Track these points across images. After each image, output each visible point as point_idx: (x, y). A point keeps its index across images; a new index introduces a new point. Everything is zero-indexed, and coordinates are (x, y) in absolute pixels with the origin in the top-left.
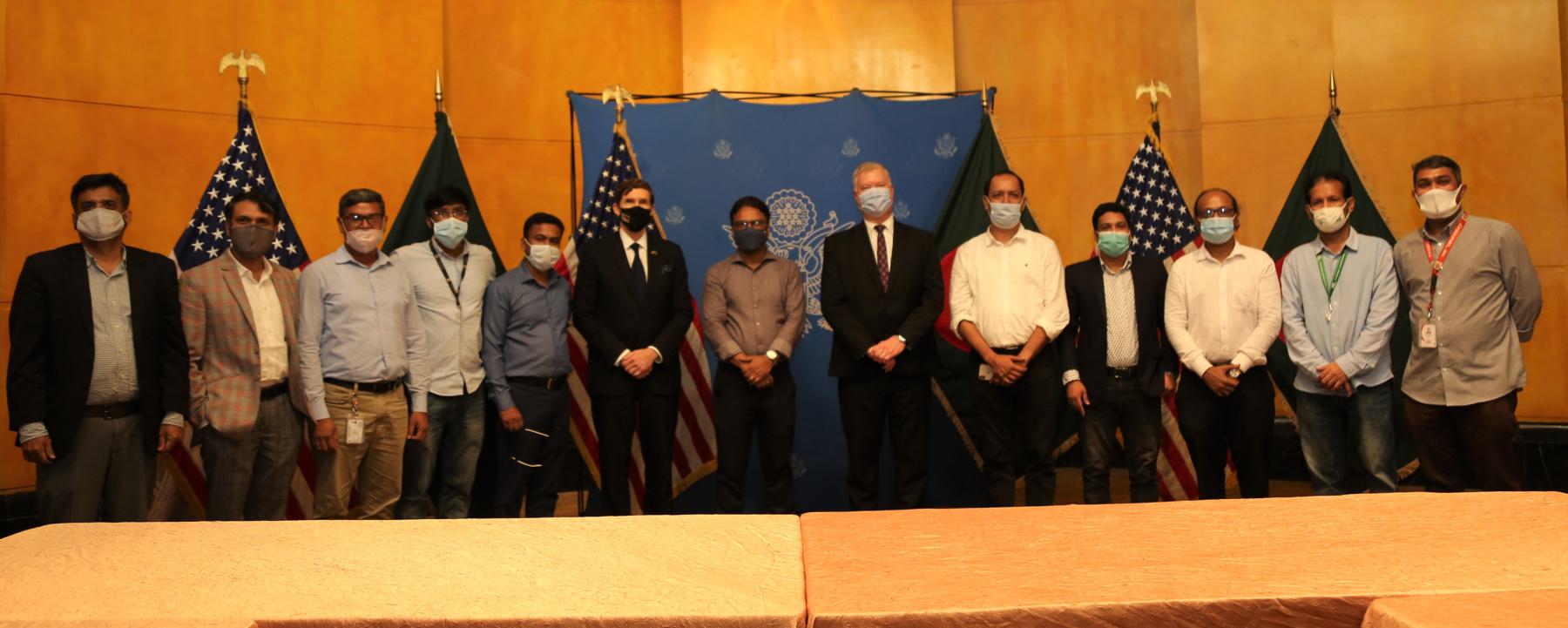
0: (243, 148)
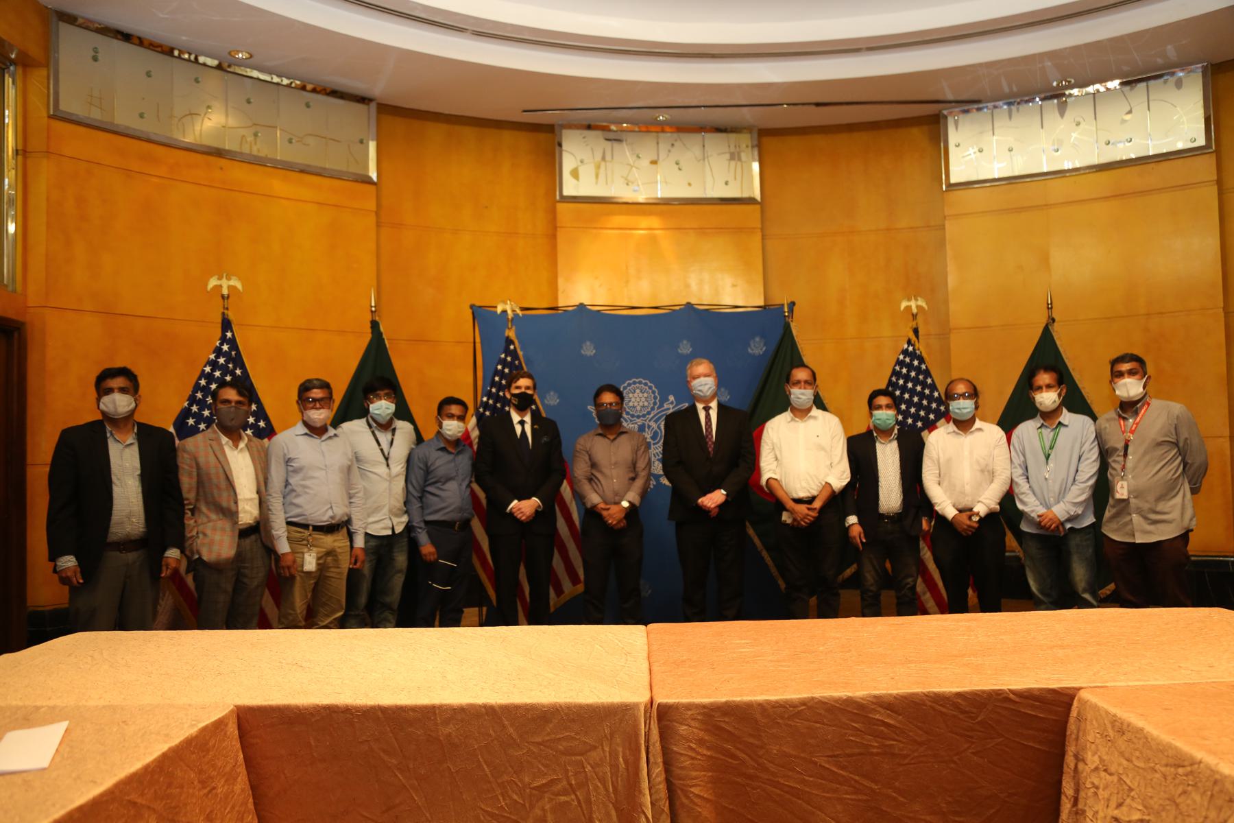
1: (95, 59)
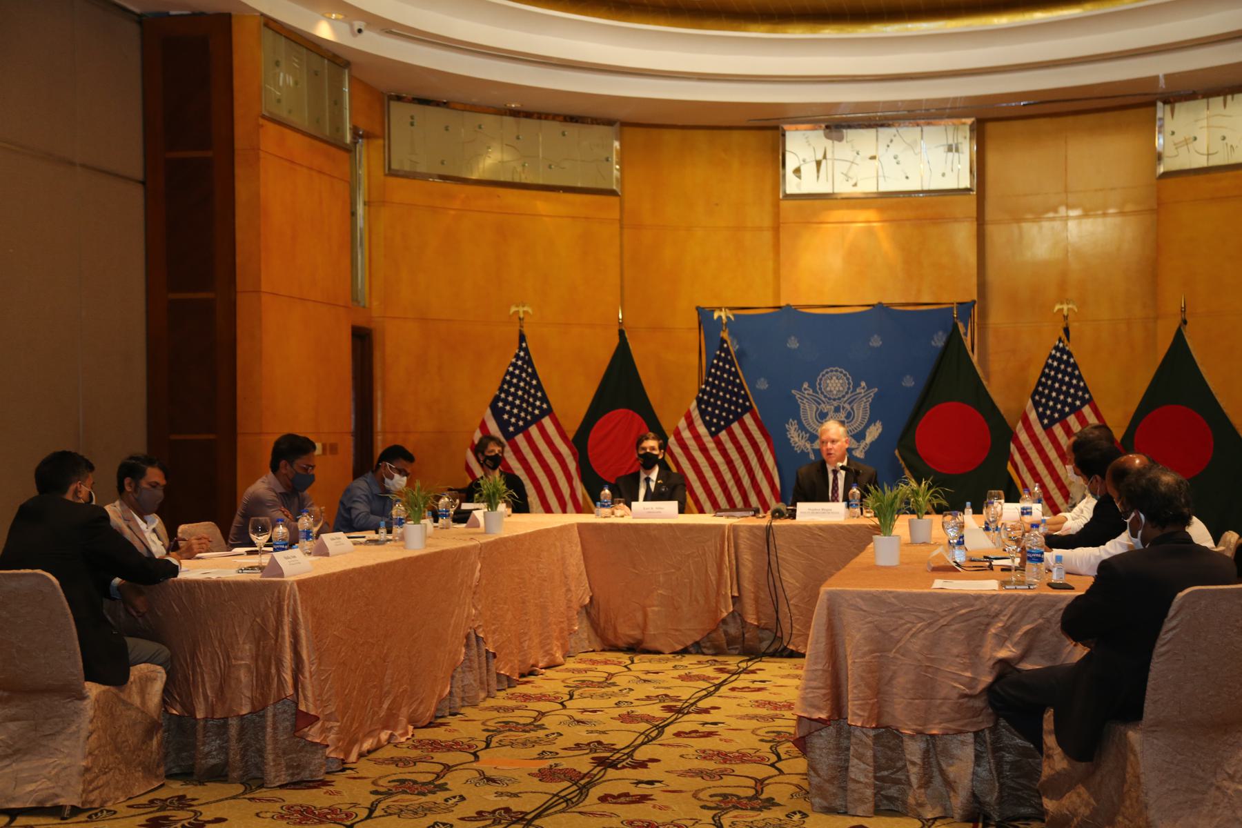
0: (522, 354)
1: (412, 124)
